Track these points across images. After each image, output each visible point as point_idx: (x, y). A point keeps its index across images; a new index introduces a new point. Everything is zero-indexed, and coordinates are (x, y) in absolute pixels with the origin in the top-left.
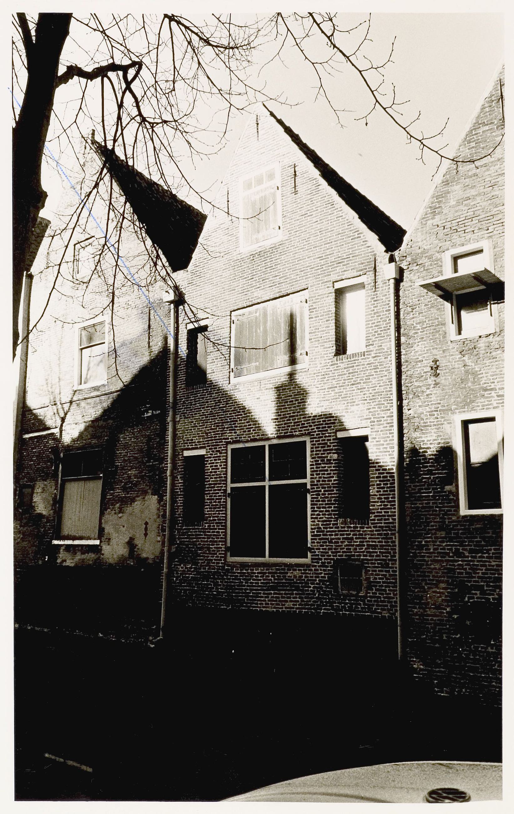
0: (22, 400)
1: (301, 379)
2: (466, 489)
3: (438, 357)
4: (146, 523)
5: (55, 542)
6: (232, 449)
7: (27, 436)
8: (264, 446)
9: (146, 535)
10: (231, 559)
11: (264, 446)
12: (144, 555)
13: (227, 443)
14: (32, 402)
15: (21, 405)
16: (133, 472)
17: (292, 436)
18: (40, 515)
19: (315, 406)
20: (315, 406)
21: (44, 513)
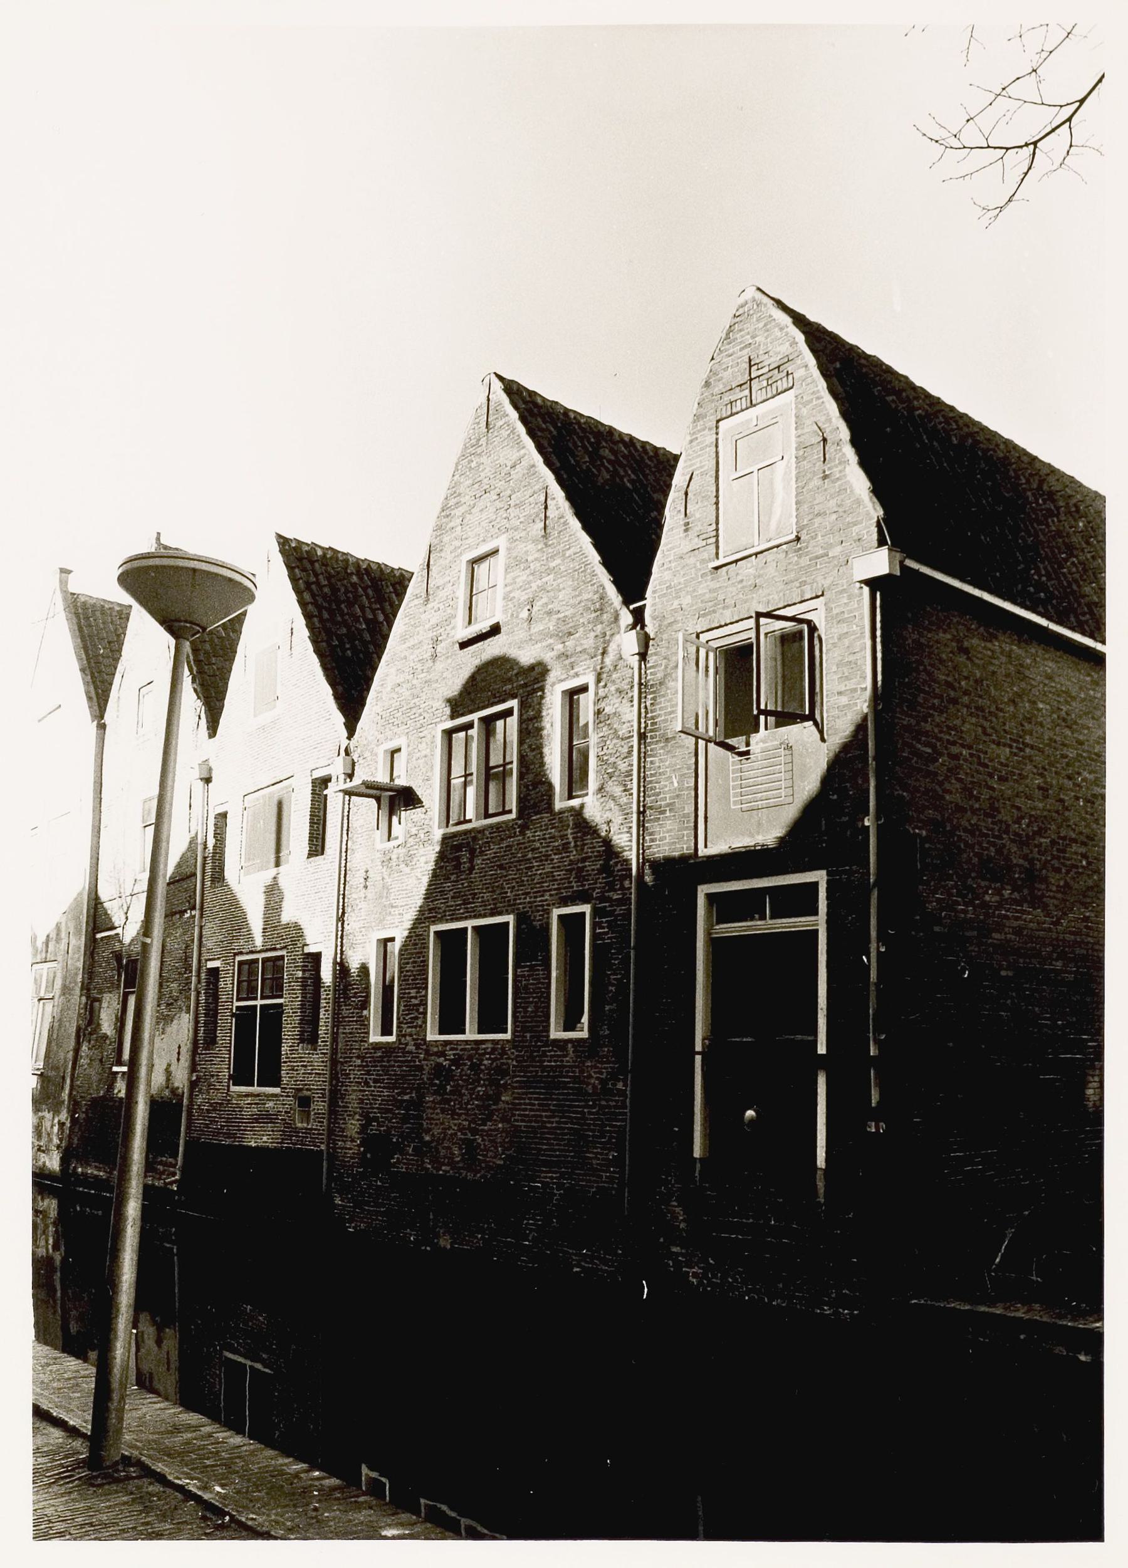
0: (93, 887)
1: (283, 883)
2: (563, 1009)
3: (746, 765)
4: (179, 1047)
5: (115, 1069)
6: (560, 917)
7: (99, 936)
8: (466, 929)
9: (178, 1060)
10: (234, 1088)
11: (466, 929)
12: (176, 1085)
13: (235, 954)
14: (103, 895)
15: (93, 896)
16: (174, 985)
17: (275, 949)
18: (105, 1037)
19: (286, 917)
20: (286, 917)
21: (109, 1033)
